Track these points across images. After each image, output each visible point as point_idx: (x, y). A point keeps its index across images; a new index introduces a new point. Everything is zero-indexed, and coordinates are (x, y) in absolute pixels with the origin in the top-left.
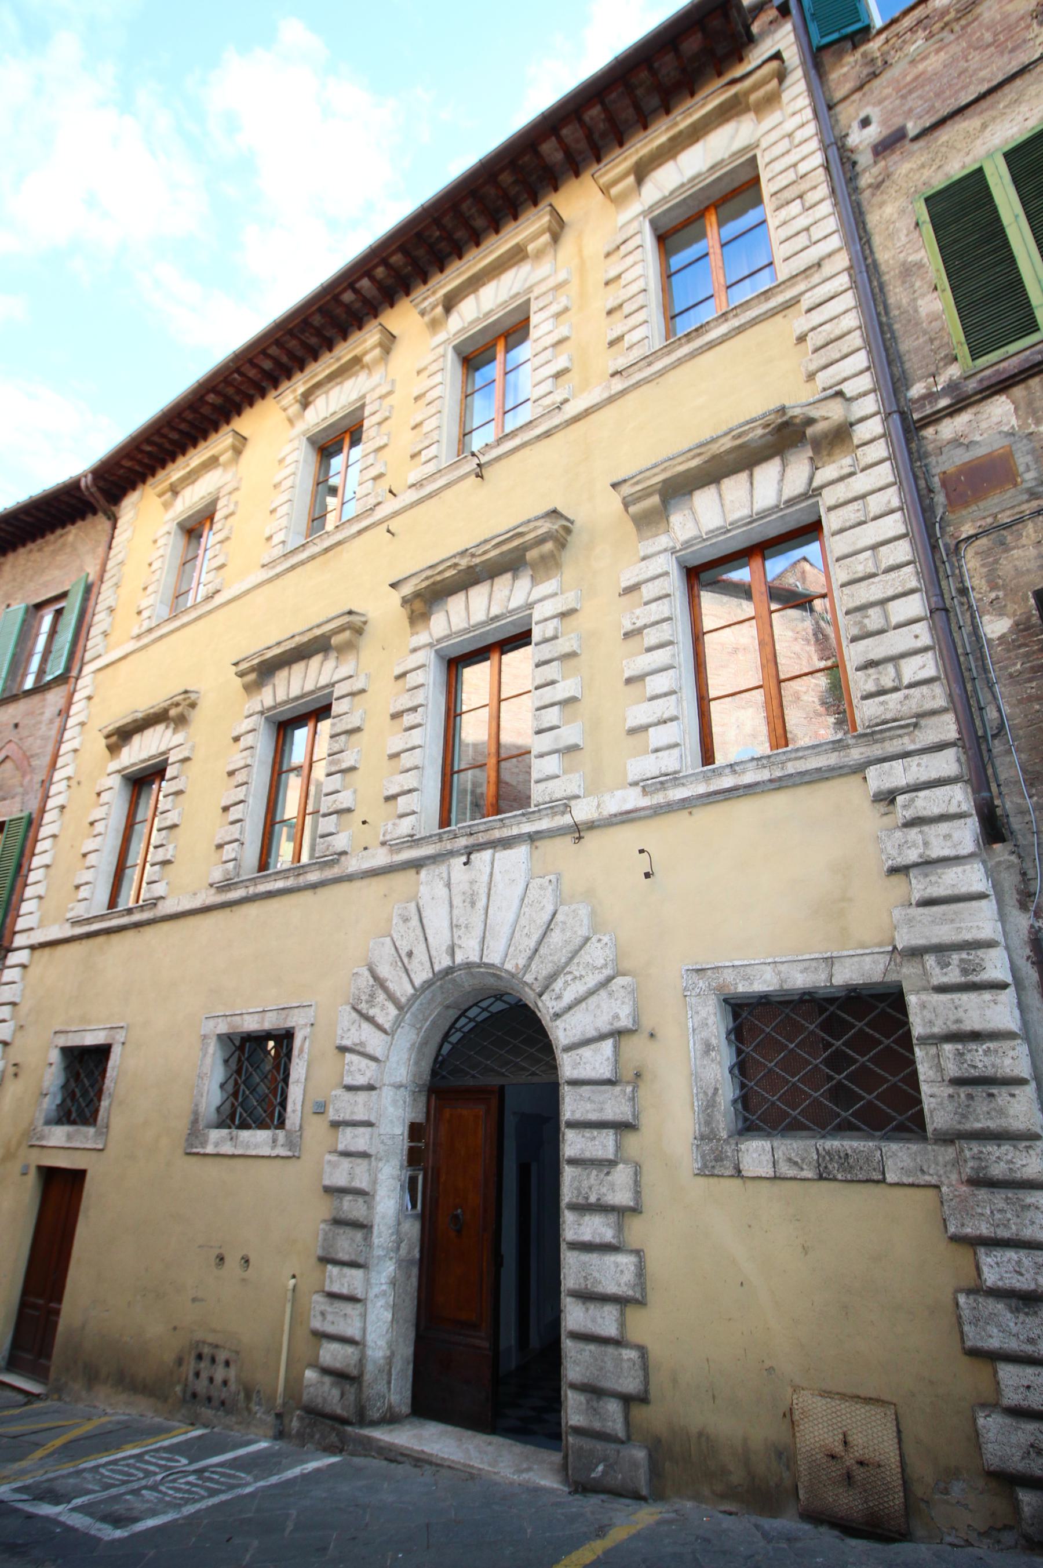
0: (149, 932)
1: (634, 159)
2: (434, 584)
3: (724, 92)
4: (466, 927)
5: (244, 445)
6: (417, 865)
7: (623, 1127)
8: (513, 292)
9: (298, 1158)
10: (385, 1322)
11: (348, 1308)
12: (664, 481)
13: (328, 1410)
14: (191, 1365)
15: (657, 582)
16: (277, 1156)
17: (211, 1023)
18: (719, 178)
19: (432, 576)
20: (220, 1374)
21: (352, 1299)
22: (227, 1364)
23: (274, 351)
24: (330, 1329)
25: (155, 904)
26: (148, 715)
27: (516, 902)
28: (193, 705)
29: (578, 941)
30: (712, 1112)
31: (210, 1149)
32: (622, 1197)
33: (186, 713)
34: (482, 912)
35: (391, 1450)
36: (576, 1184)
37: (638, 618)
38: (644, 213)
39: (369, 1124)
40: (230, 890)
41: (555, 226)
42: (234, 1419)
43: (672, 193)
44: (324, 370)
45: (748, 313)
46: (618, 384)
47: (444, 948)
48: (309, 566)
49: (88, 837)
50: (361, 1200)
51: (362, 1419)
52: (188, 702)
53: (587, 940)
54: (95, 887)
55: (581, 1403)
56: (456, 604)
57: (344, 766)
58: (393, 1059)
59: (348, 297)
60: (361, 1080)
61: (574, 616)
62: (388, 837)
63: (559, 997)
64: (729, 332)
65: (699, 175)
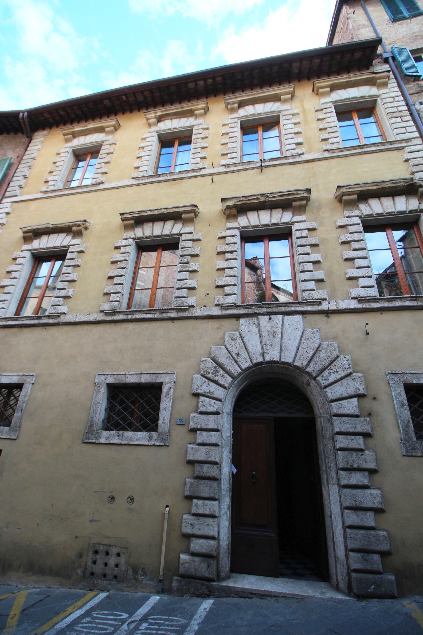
0: (53, 330)
1: (332, 83)
2: (244, 204)
3: (369, 75)
4: (271, 345)
5: (119, 128)
6: (238, 317)
7: (367, 435)
8: (272, 110)
9: (168, 446)
10: (226, 527)
11: (210, 521)
12: (361, 191)
13: (199, 574)
14: (91, 556)
15: (356, 226)
16: (153, 445)
17: (103, 378)
18: (362, 102)
19: (244, 200)
20: (112, 561)
21: (213, 516)
22: (118, 555)
23: (147, 93)
24: (197, 532)
25: (59, 316)
26: (56, 227)
27: (298, 338)
28: (86, 228)
29: (334, 357)
30: (408, 430)
31: (102, 441)
32: (371, 465)
33: (82, 230)
34: (280, 340)
35: (244, 592)
36: (346, 459)
37: (348, 237)
38: (157, 132)
39: (217, 430)
40: (115, 315)
41: (206, 109)
42: (125, 585)
43: (345, 99)
44: (174, 109)
45: (383, 146)
46: (327, 155)
47: (259, 353)
48: (162, 184)
49: (8, 279)
50: (215, 466)
51: (219, 578)
52: (84, 226)
53: (338, 357)
54: (10, 303)
55: (359, 558)
56: (44, 238)
57: (190, 269)
58: (227, 401)
59: (191, 85)
60: (211, 410)
61: (315, 231)
62: (220, 303)
63: (326, 379)
64: (377, 150)
65: (356, 98)
